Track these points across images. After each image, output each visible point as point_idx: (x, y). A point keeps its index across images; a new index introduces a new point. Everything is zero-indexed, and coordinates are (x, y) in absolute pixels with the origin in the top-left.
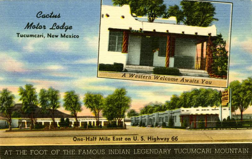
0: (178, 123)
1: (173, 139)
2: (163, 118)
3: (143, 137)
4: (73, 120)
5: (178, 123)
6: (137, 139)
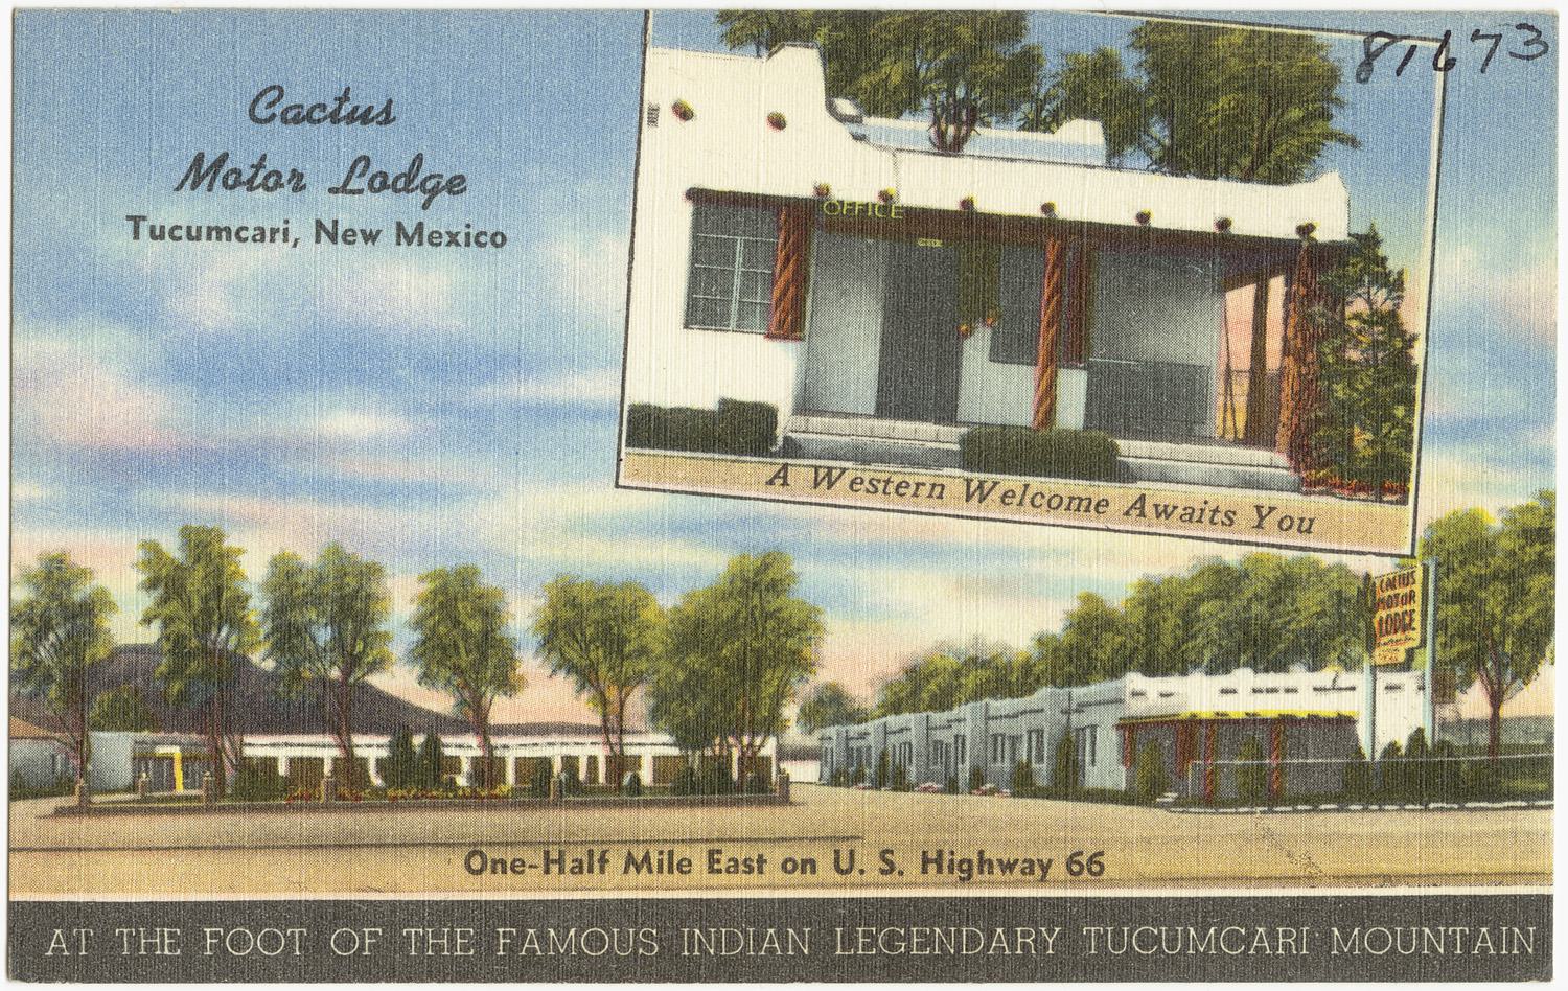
0: (1106, 767)
1: (476, 863)
2: (1015, 740)
3: (892, 852)
4: (464, 749)
5: (1106, 767)
6: (858, 866)
